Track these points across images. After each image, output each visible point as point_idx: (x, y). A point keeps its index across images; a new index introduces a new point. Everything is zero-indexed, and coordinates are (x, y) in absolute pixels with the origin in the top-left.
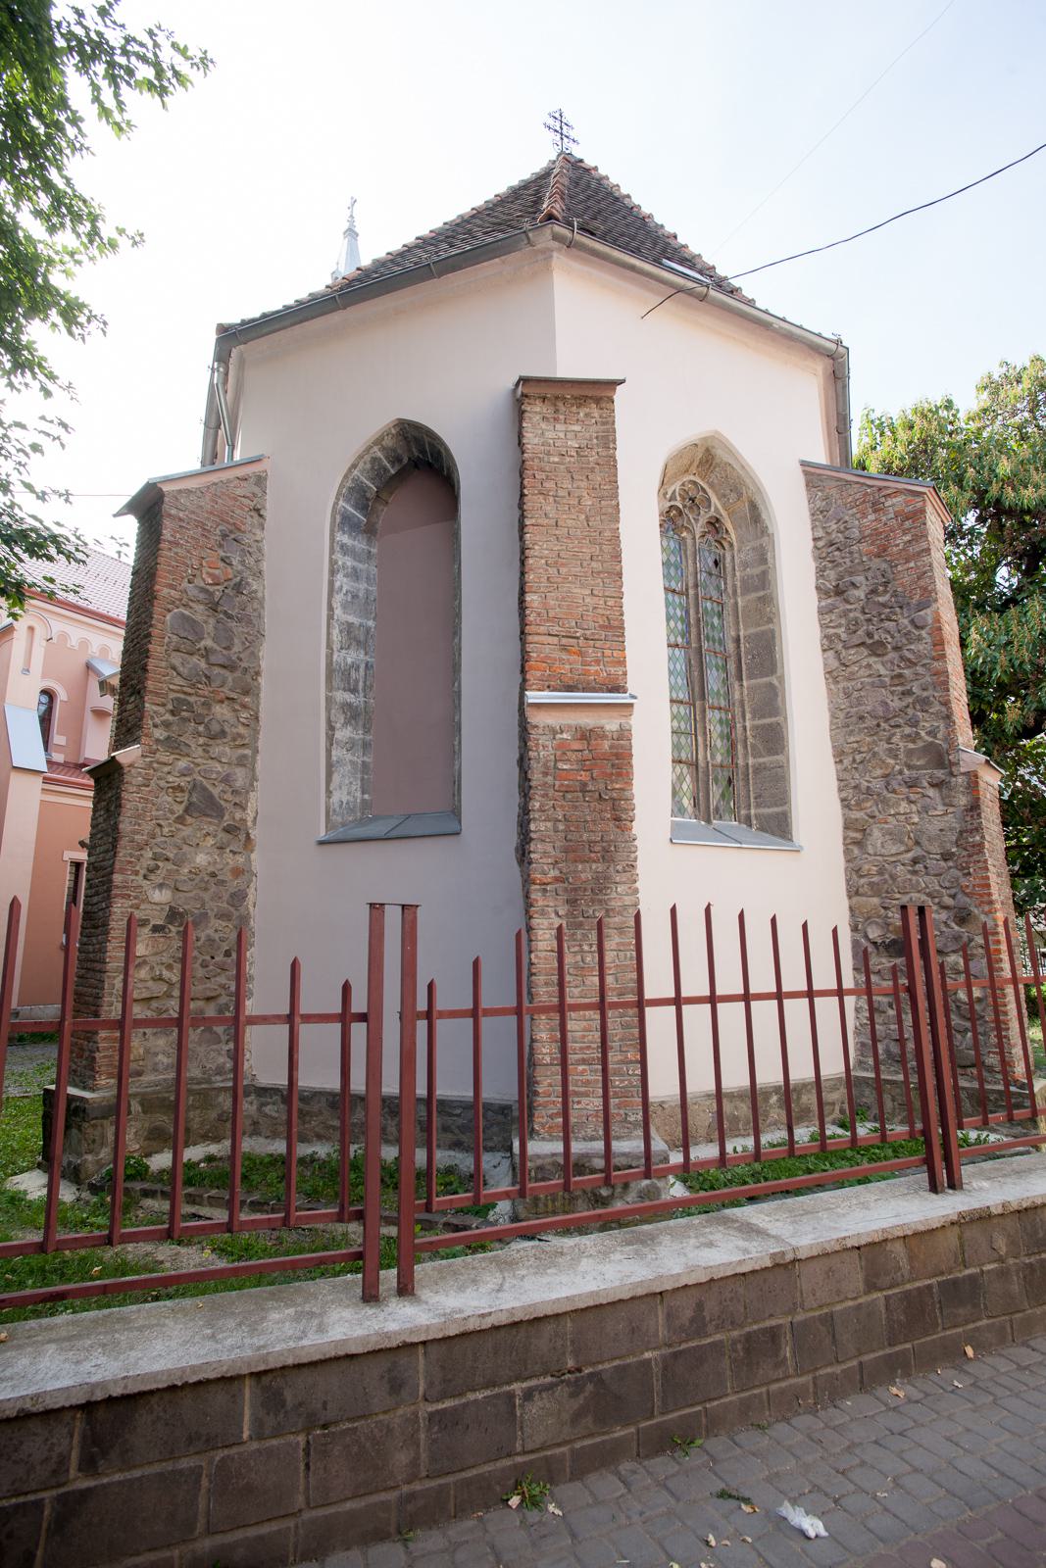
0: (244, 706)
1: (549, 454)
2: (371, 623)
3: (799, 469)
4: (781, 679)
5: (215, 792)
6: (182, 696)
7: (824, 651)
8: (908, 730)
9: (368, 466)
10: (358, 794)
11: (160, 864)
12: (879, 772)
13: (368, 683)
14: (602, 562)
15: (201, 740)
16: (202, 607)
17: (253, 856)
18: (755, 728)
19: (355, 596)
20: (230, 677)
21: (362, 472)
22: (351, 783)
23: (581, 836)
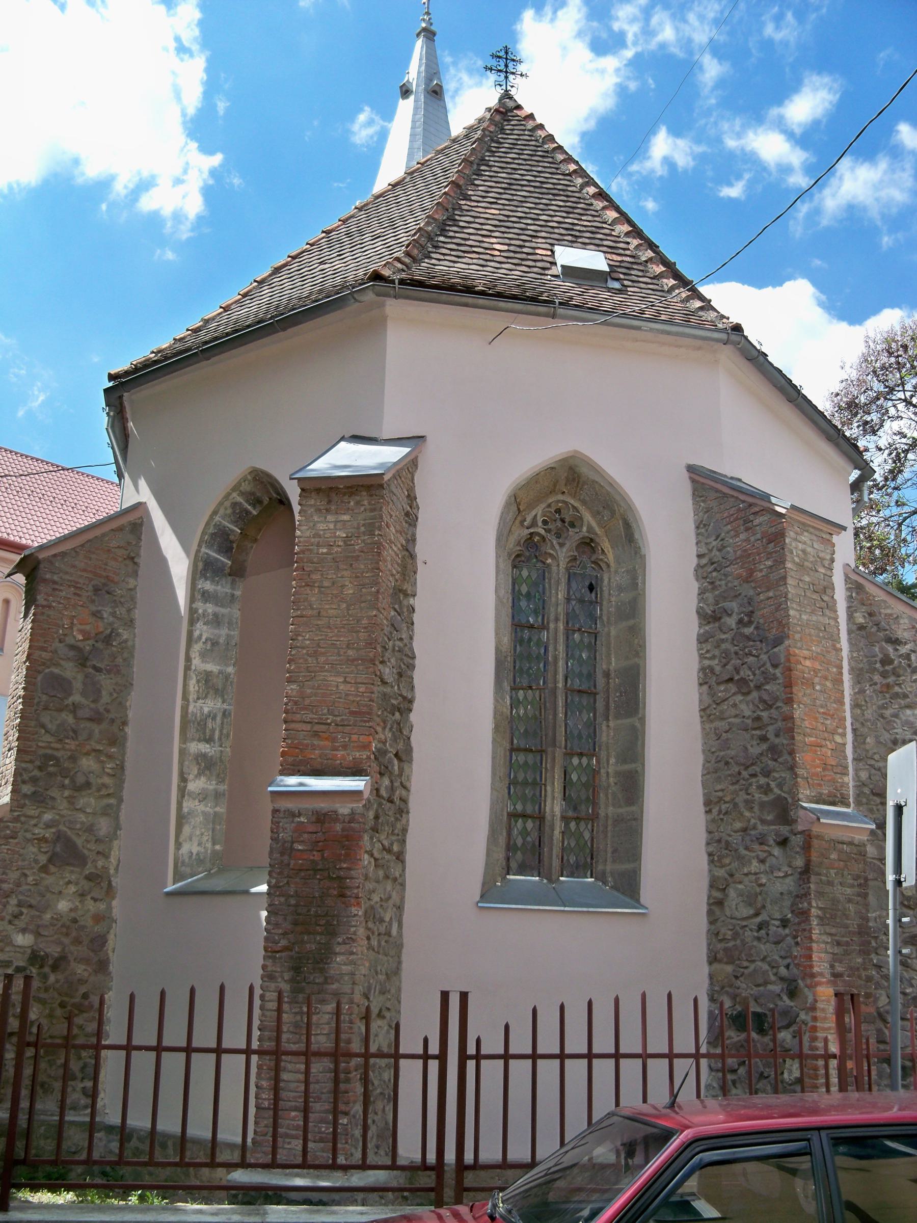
0: (110, 757)
1: (318, 545)
2: (230, 670)
3: (686, 475)
4: (643, 720)
5: (79, 842)
6: (49, 752)
7: (701, 685)
8: (763, 780)
9: (229, 511)
10: (209, 845)
11: (24, 910)
12: (738, 825)
13: (225, 732)
14: (358, 650)
15: (67, 793)
16: (71, 664)
17: (114, 903)
18: (618, 774)
19: (215, 643)
20: (96, 729)
21: (223, 518)
22: (202, 834)
23: (309, 911)
